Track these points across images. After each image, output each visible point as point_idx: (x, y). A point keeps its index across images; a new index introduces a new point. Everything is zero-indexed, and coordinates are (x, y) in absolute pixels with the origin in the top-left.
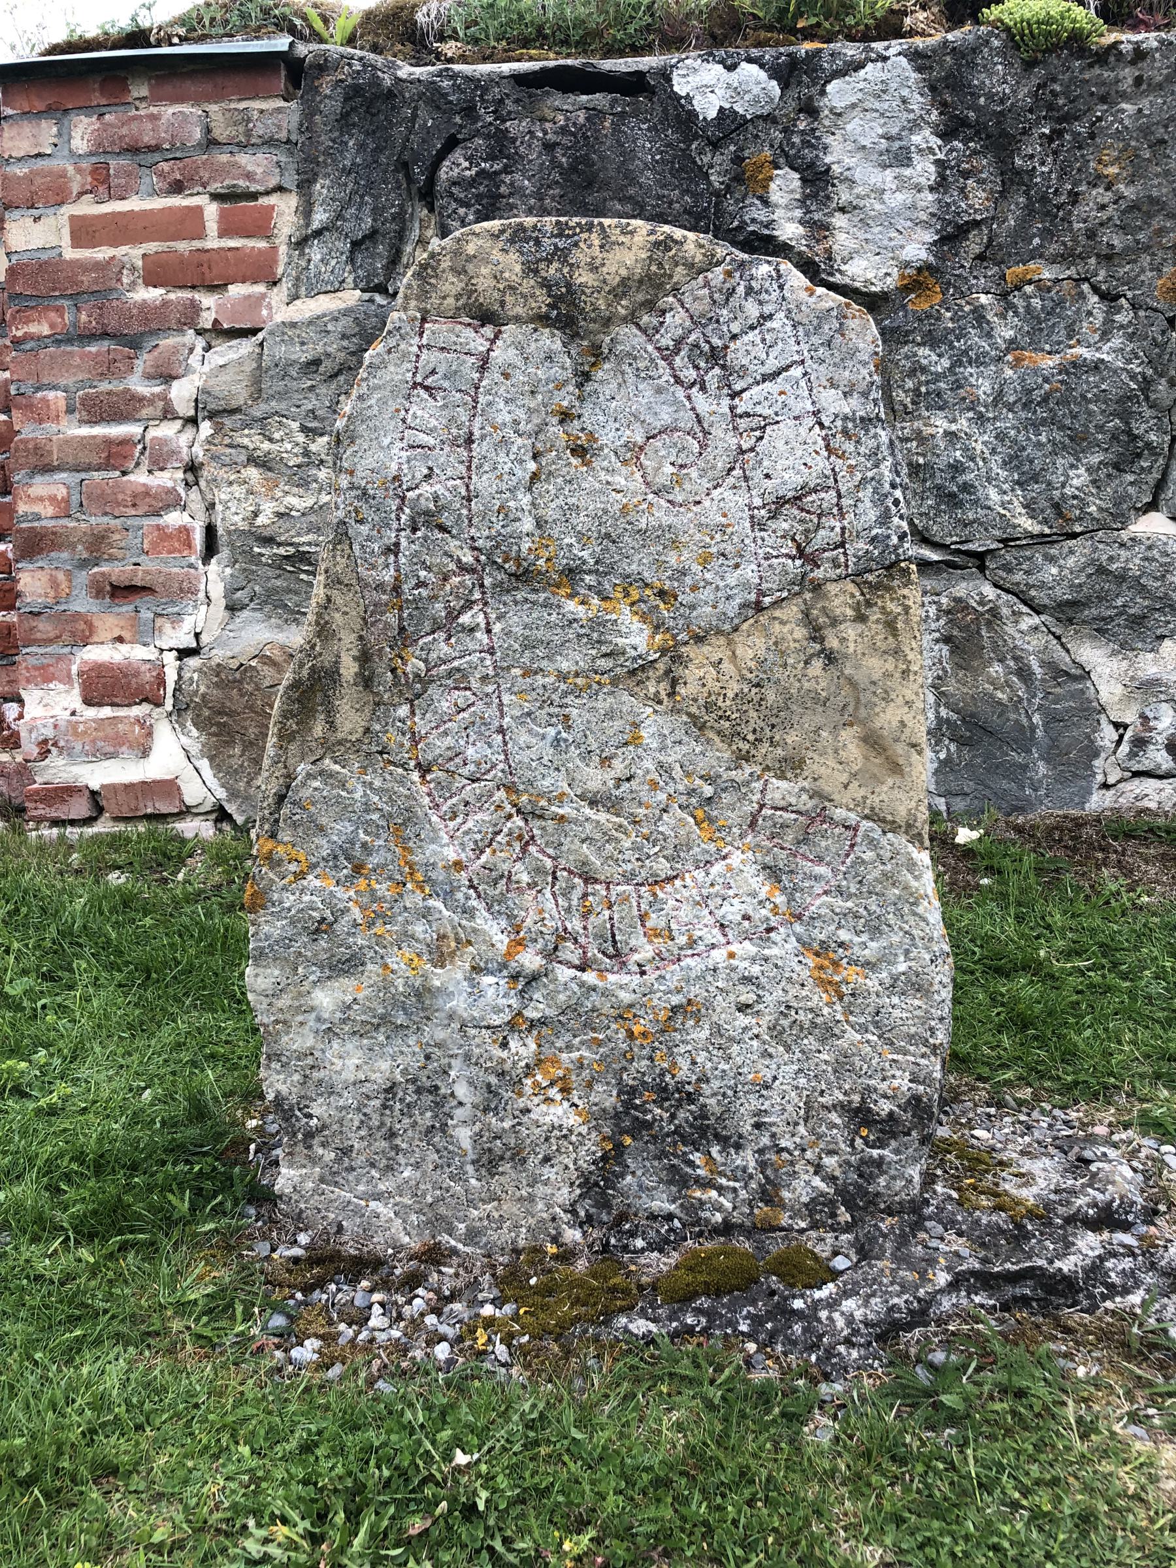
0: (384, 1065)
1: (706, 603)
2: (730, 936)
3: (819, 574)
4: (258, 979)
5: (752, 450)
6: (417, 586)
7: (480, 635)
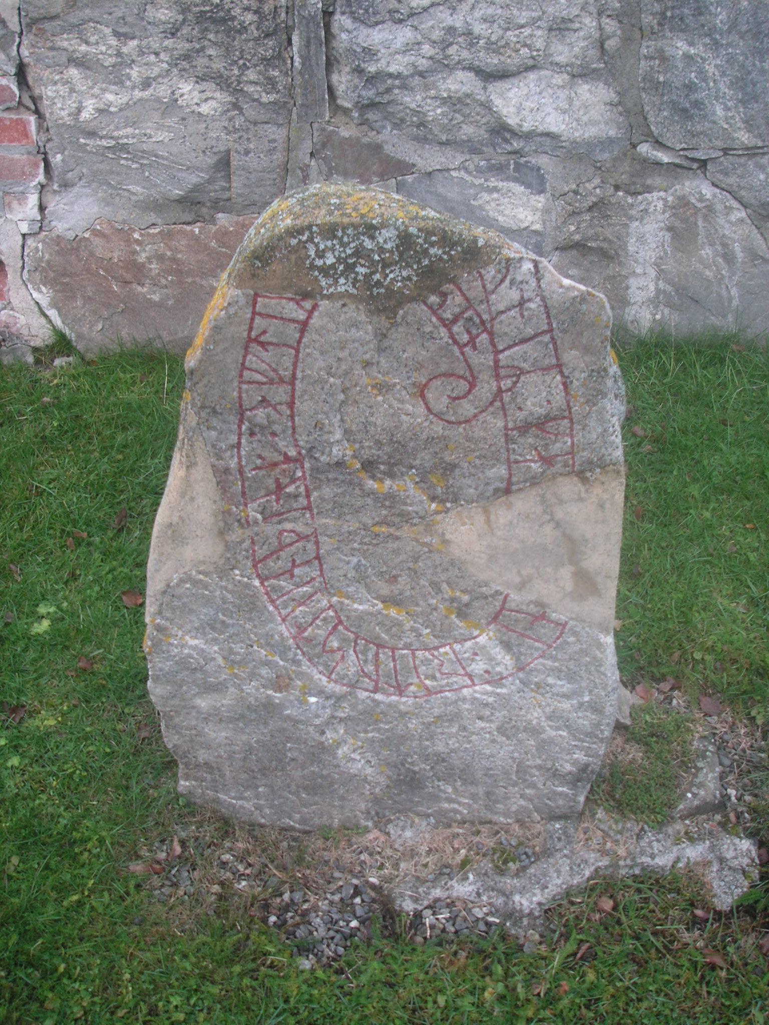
5: (509, 390)
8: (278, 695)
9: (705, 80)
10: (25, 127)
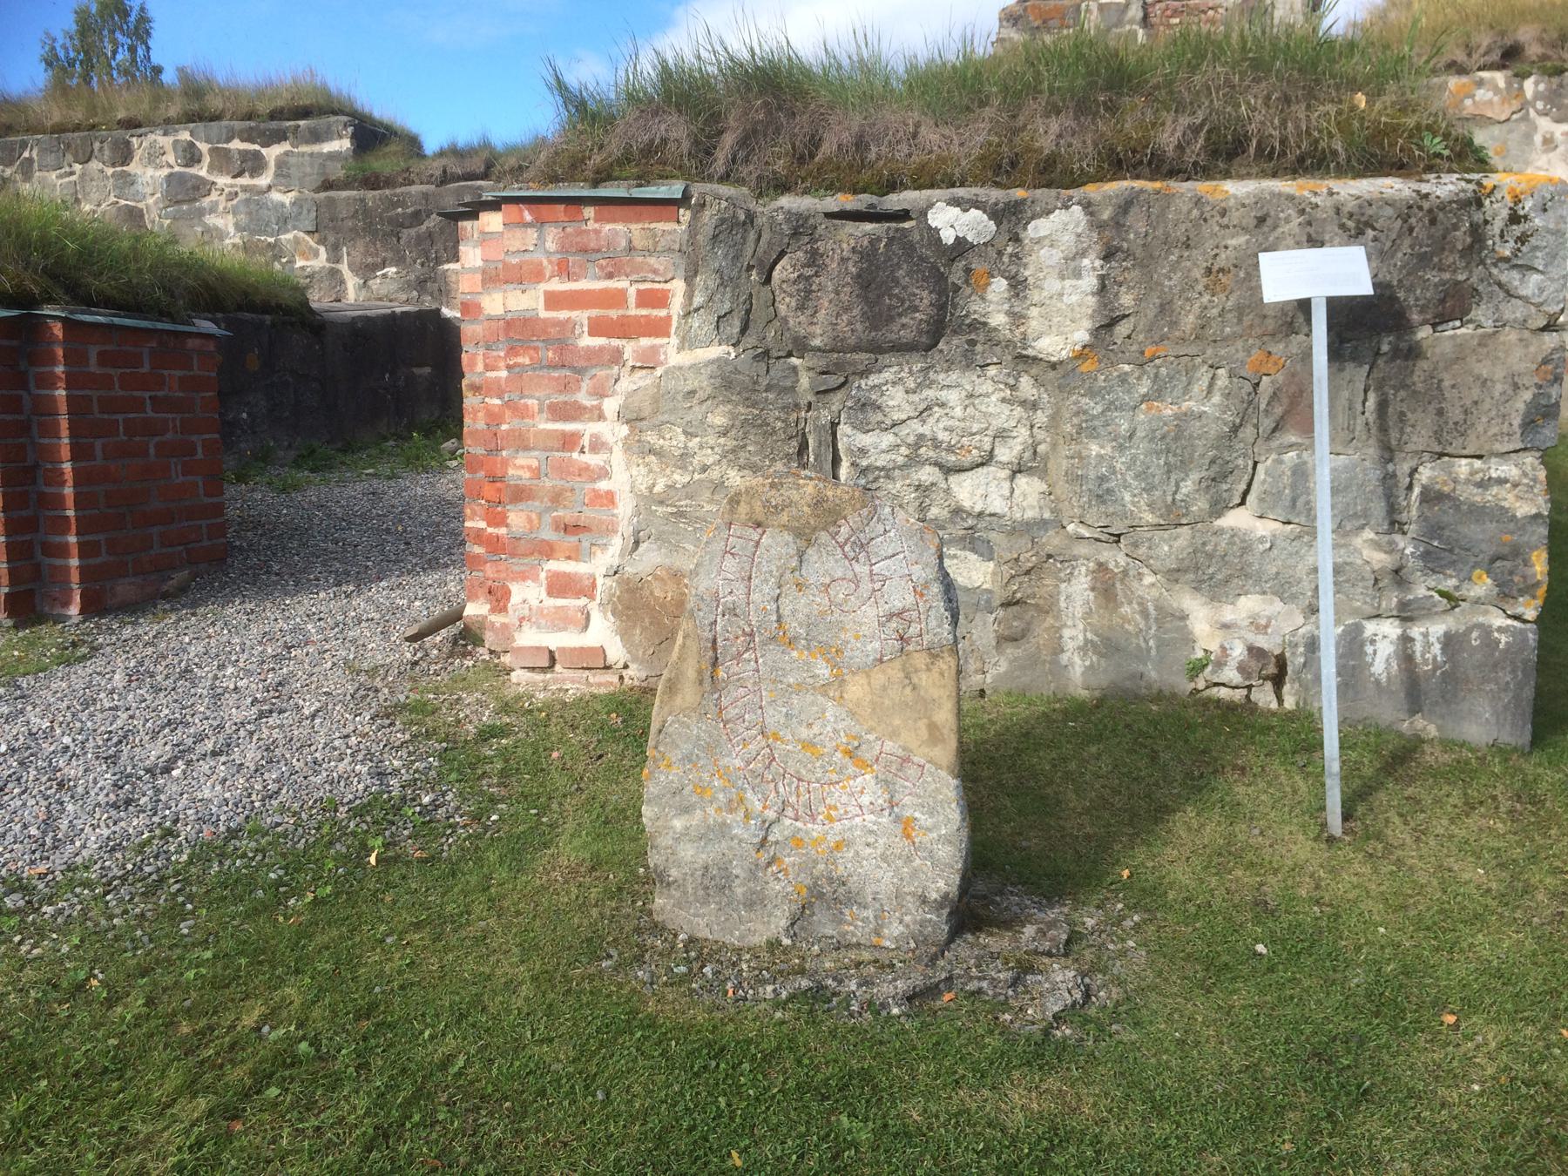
3: (910, 648)
4: (647, 811)
9: (1114, 473)
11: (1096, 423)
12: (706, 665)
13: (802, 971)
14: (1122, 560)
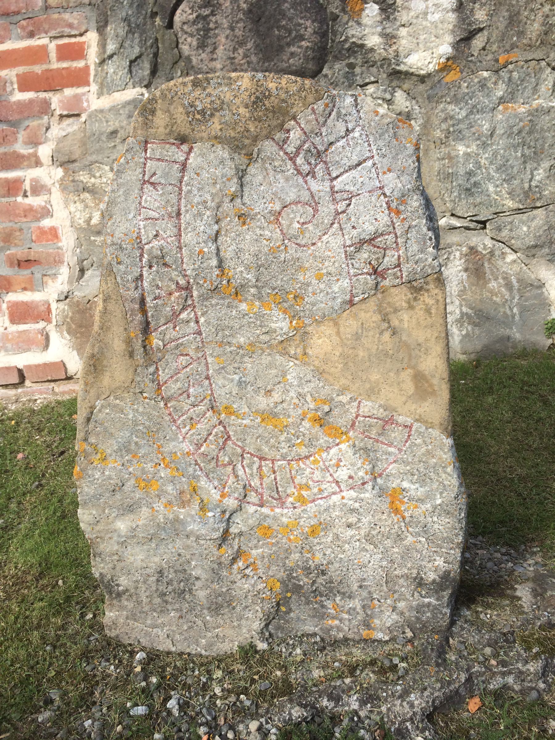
0: (157, 559)
1: (322, 302)
2: (342, 487)
3: (386, 283)
4: (84, 516)
5: (344, 212)
6: (155, 299)
7: (192, 324)
8: (182, 510)
9: (480, 167)
10: (56, 232)
11: (461, 126)
12: (135, 331)
13: (286, 689)
14: (489, 243)
